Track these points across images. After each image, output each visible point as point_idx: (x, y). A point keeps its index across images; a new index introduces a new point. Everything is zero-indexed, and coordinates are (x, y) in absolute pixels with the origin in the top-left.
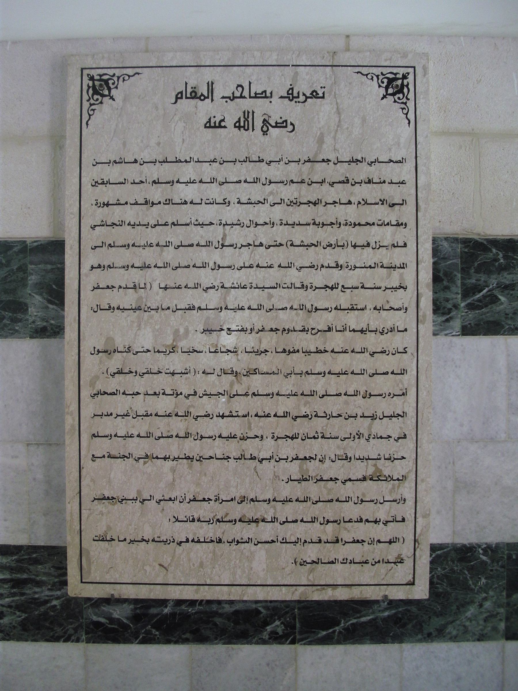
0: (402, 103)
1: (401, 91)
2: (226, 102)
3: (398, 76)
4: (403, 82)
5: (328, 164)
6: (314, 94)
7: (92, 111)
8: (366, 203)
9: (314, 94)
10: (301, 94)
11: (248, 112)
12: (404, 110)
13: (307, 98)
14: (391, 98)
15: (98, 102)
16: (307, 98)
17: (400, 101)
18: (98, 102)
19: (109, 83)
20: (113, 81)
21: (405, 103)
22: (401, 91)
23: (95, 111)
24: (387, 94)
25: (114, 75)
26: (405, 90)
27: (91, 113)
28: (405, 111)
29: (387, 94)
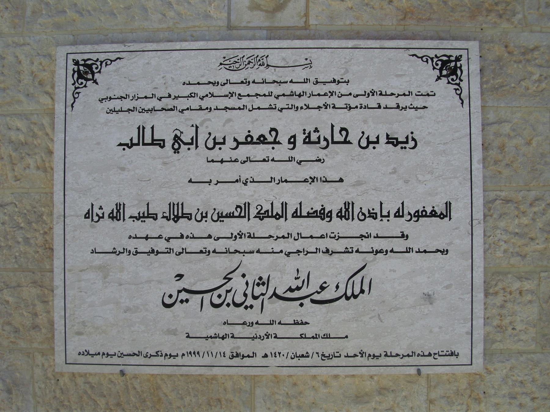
0: (101, 65)
1: (90, 67)
2: (134, 221)
3: (76, 69)
4: (82, 65)
5: (299, 255)
6: (262, 139)
7: (425, 60)
8: (213, 96)
9: (262, 139)
10: (322, 139)
11: (174, 204)
12: (108, 63)
13: (239, 143)
14: (97, 76)
15: (434, 65)
16: (239, 143)
17: (99, 67)
18: (434, 65)
19: (453, 75)
20: (455, 79)
21: (102, 62)
22: (90, 67)
23: (426, 63)
24: (93, 79)
25: (461, 81)
26: (89, 62)
27: (424, 59)
28: (109, 62)
29: (93, 79)
